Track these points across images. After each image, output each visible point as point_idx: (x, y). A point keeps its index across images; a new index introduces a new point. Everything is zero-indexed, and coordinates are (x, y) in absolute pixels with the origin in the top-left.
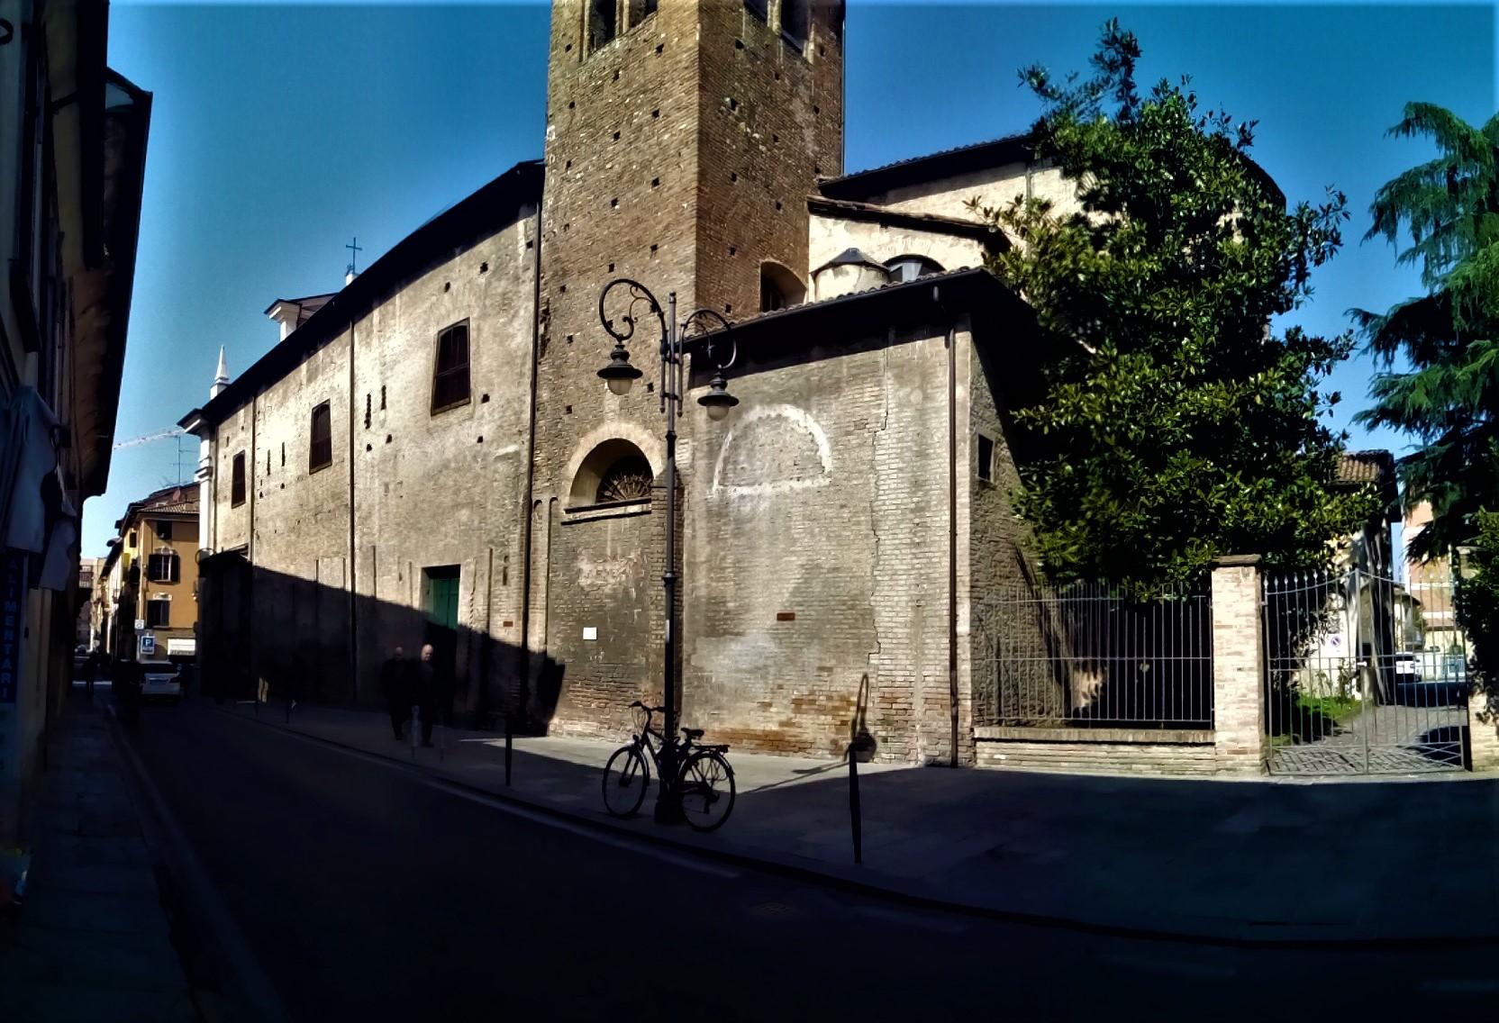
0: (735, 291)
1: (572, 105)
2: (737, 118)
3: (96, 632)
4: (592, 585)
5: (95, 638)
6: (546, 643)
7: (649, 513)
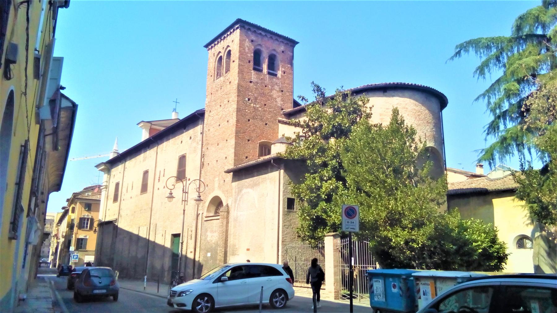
1: (212, 94)
2: (250, 103)
3: (53, 252)
4: (210, 240)
5: (52, 255)
6: (199, 258)
7: (219, 219)
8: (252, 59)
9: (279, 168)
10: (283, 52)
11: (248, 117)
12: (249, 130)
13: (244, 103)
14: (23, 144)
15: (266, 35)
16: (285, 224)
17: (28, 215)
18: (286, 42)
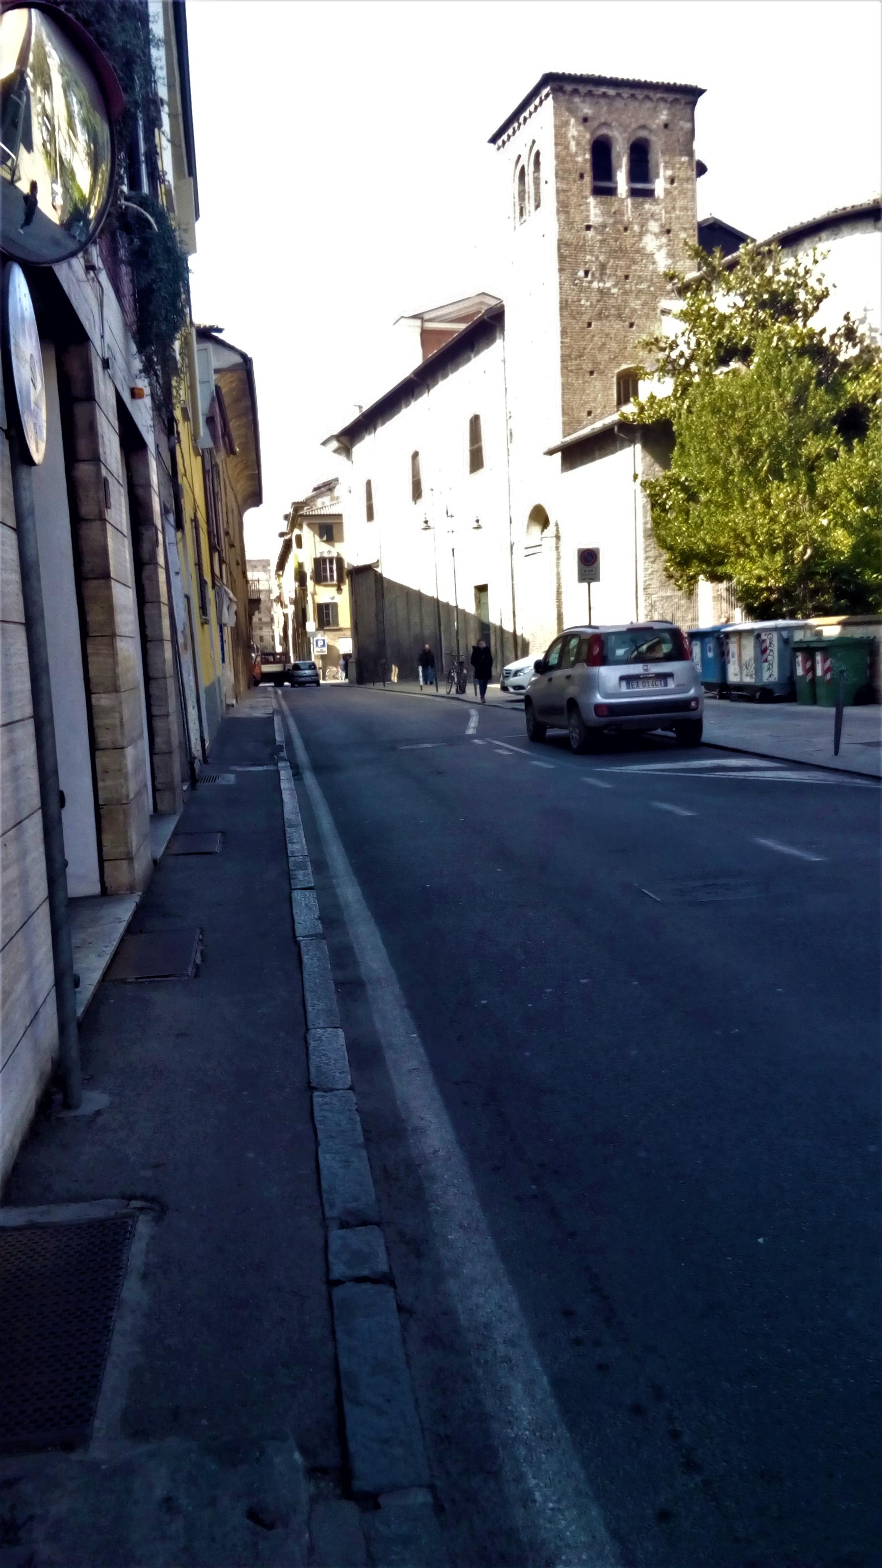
0: (595, 400)
8: (588, 167)
9: (632, 442)
10: (666, 126)
11: (586, 318)
12: (592, 349)
13: (576, 285)
14: (193, 518)
15: (619, 95)
16: (648, 554)
17: (214, 586)
18: (671, 97)
